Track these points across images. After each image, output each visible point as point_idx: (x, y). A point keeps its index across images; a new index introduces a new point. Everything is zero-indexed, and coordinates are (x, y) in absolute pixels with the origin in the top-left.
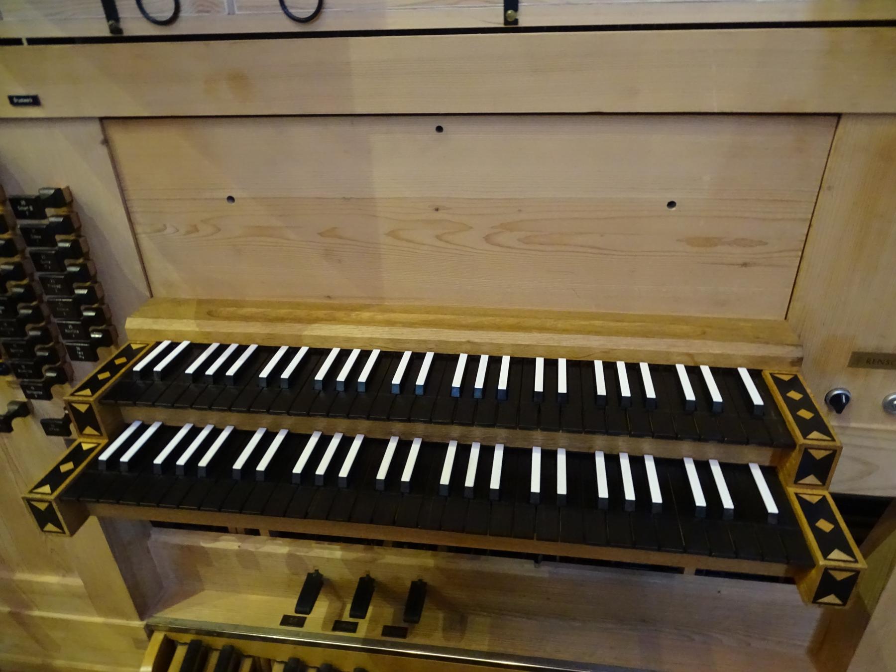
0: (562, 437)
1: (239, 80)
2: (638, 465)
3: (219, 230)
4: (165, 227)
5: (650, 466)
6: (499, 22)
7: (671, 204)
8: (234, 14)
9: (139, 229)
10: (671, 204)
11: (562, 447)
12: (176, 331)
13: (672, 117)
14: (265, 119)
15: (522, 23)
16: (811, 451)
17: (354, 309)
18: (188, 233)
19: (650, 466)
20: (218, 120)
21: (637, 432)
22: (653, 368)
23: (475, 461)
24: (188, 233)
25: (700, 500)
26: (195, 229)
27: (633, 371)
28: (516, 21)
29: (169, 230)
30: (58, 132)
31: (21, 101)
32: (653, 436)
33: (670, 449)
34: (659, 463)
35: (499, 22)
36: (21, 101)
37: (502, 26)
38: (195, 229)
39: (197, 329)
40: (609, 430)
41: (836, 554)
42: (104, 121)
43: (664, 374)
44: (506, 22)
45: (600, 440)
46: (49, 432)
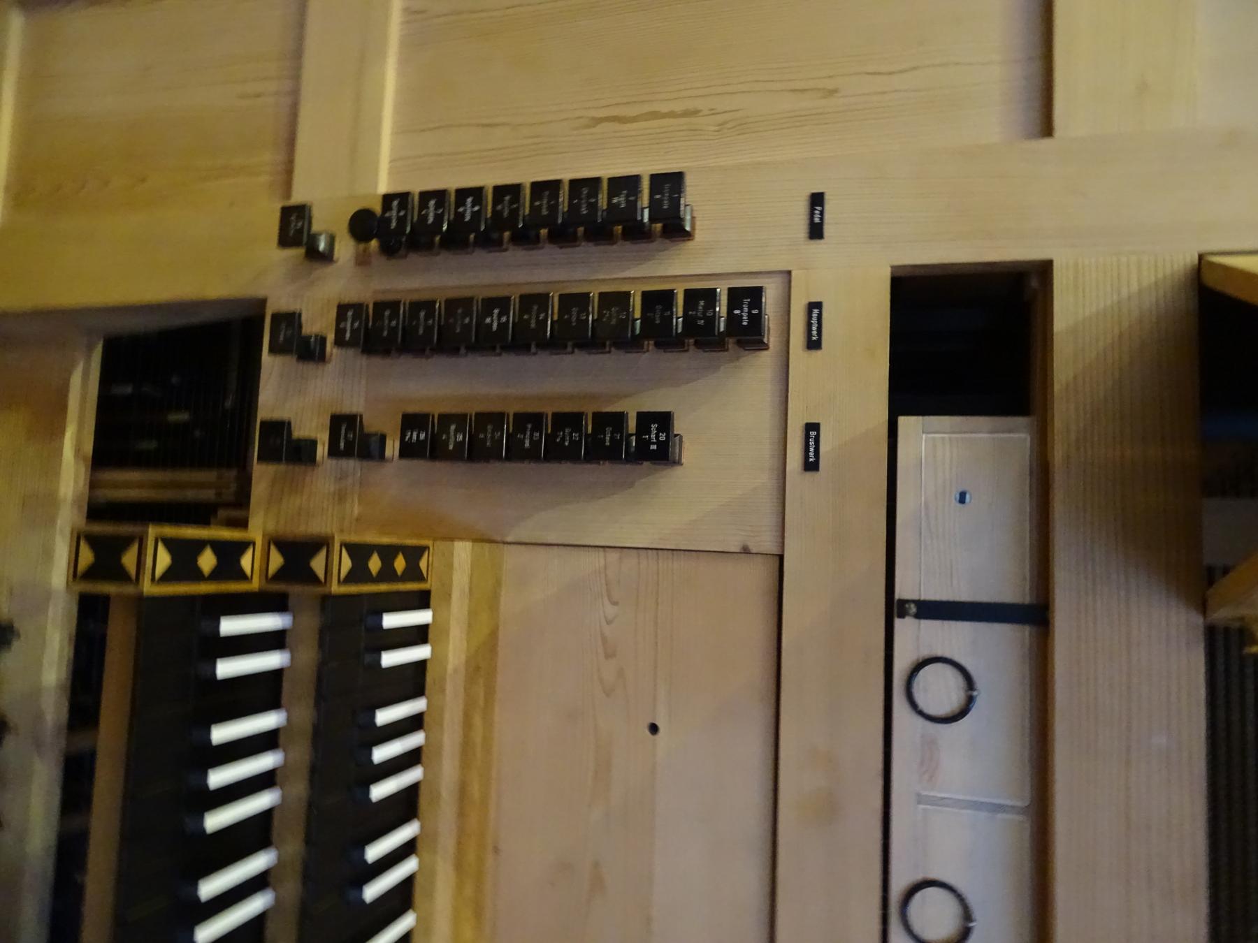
0: (309, 655)
1: (828, 809)
2: (263, 781)
3: (608, 695)
4: (615, 604)
5: (270, 661)
6: (901, 592)
7: (654, 729)
8: (919, 803)
9: (613, 556)
10: (654, 729)
11: (292, 659)
12: (447, 632)
13: (770, 756)
14: (769, 785)
15: (898, 623)
16: (323, 553)
17: (478, 913)
18: (604, 640)
19: (270, 661)
20: (772, 731)
21: (317, 774)
22: (421, 666)
23: (249, 771)
24: (604, 640)
25: (222, 733)
26: (609, 655)
27: (418, 635)
28: (902, 615)
29: (611, 610)
30: (764, 480)
31: (812, 443)
32: (322, 666)
33: (299, 691)
34: (265, 817)
35: (901, 592)
36: (812, 443)
37: (897, 597)
38: (609, 655)
39: (450, 668)
40: (320, 736)
41: (165, 559)
42: (777, 560)
43: (412, 680)
44: (903, 603)
45: (305, 714)
46: (286, 240)
